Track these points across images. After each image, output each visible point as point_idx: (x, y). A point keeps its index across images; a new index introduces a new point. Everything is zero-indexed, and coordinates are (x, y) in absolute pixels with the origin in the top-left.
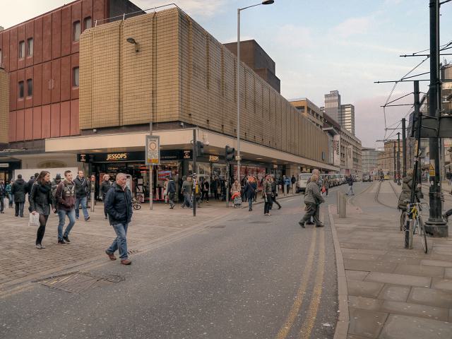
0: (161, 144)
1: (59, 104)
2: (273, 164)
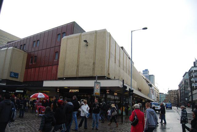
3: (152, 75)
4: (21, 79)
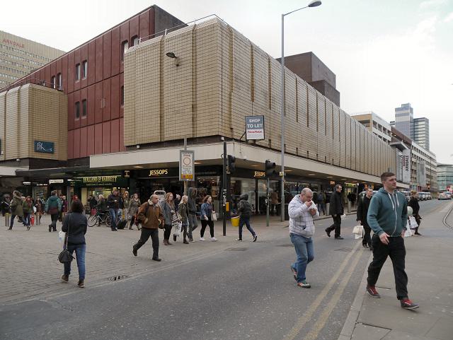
0: (195, 159)
1: (118, 120)
2: (330, 180)
4: (60, 154)
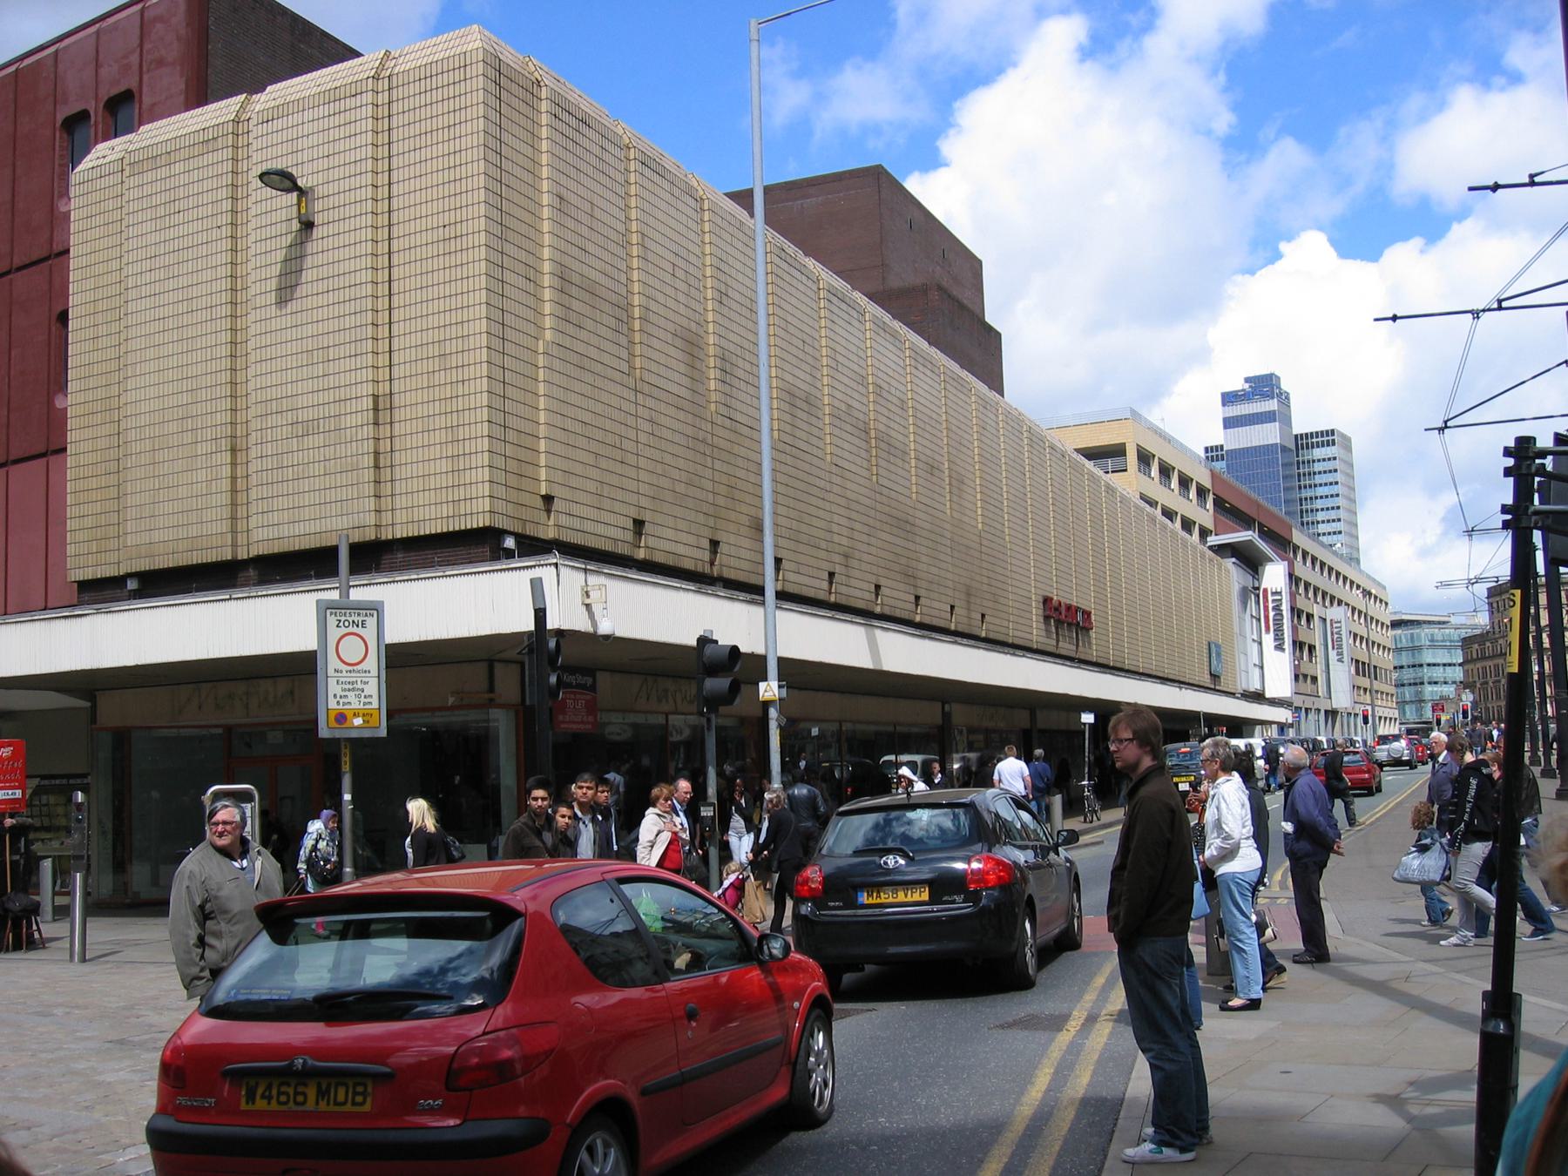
3: (1327, 437)
